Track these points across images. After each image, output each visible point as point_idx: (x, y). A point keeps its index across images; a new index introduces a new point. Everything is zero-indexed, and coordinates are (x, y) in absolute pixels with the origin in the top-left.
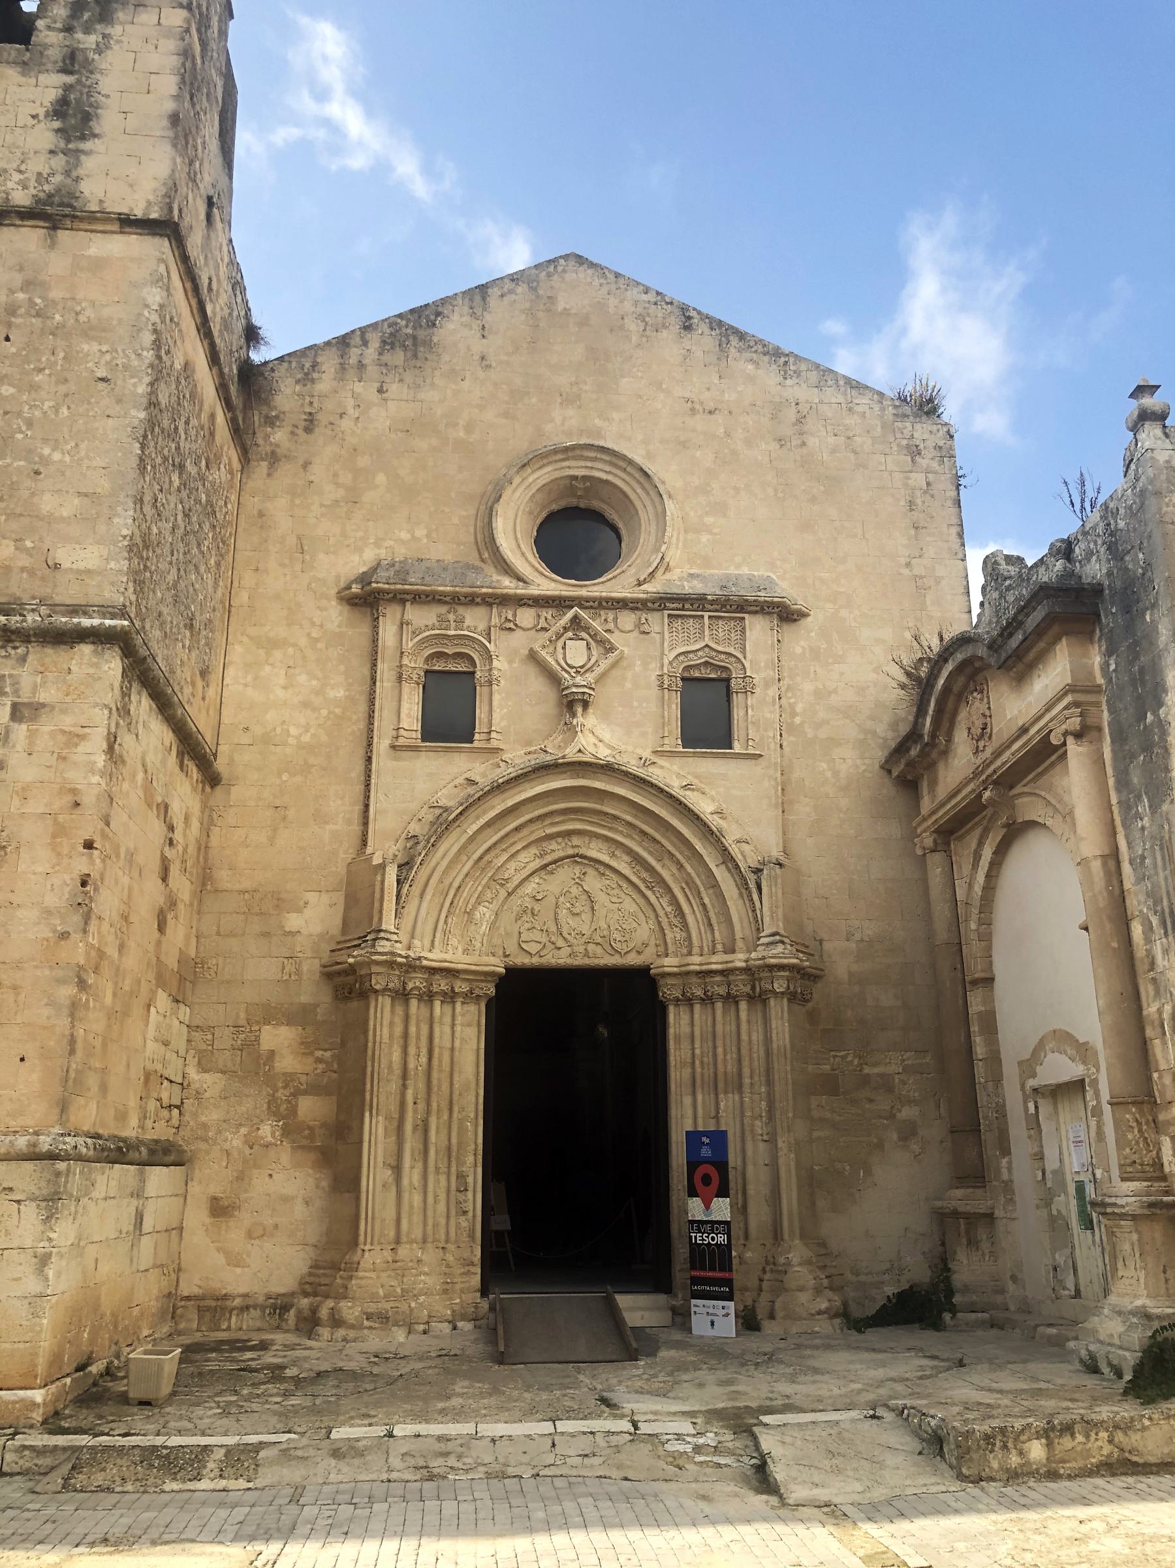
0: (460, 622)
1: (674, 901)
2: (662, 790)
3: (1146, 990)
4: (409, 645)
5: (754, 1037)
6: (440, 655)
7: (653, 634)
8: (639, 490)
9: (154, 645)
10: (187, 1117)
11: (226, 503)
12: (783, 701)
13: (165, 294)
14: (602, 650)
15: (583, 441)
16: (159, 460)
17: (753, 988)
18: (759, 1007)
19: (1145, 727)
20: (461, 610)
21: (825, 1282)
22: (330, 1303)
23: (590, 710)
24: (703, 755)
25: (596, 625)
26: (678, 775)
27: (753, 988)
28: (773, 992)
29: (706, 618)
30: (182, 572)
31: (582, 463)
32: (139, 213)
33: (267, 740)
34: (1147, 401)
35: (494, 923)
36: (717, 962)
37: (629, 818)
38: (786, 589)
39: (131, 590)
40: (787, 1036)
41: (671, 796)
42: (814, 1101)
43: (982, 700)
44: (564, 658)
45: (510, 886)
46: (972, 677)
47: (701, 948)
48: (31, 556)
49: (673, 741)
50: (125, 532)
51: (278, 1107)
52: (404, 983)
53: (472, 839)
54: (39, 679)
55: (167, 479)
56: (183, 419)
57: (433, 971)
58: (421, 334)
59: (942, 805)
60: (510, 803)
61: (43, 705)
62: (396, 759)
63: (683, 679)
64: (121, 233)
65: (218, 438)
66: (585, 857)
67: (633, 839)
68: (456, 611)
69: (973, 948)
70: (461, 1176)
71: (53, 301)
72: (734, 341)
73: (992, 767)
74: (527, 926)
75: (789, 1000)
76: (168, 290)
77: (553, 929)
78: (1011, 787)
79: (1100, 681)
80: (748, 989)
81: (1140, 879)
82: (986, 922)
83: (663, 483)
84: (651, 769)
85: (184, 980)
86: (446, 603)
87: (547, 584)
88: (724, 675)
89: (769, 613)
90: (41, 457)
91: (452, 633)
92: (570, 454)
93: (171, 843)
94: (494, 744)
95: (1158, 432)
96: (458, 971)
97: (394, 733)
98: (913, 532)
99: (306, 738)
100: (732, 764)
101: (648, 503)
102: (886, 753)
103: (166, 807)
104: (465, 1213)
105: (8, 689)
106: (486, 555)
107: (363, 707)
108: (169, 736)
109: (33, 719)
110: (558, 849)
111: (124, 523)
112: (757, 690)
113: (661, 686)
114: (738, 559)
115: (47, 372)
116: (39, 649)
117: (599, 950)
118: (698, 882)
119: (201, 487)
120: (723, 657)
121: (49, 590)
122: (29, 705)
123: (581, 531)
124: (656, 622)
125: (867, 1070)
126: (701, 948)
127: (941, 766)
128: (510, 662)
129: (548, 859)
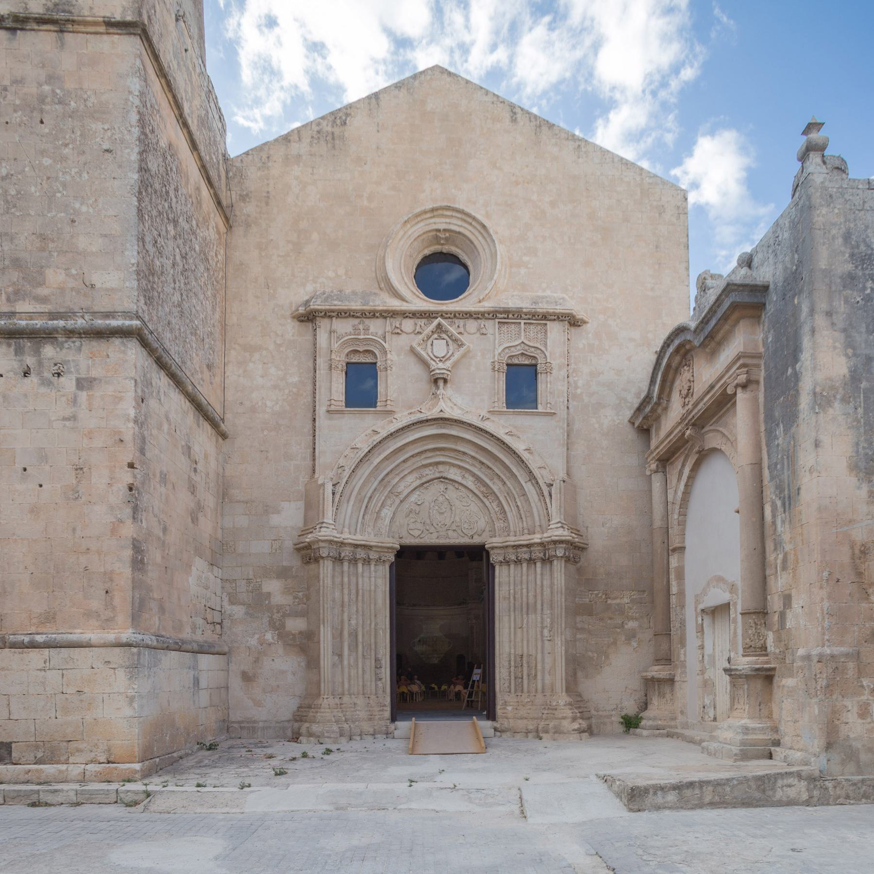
0: (367, 329)
1: (500, 504)
2: (493, 436)
3: (770, 546)
4: (335, 346)
5: (545, 583)
6: (356, 352)
7: (488, 335)
8: (480, 238)
9: (167, 344)
10: (225, 629)
11: (216, 255)
12: (571, 379)
13: (143, 84)
14: (456, 346)
15: (445, 204)
16: (154, 213)
17: (545, 555)
18: (548, 566)
19: (787, 377)
20: (367, 321)
21: (578, 715)
22: (307, 725)
23: (449, 385)
24: (519, 413)
25: (452, 330)
26: (503, 427)
27: (545, 555)
28: (556, 556)
29: (522, 324)
30: (184, 297)
31: (444, 220)
32: (118, 18)
33: (253, 410)
34: (814, 136)
35: (392, 518)
36: (524, 539)
37: (473, 454)
38: (572, 305)
39: (143, 302)
40: (563, 581)
41: (498, 439)
42: (578, 619)
43: (689, 371)
44: (432, 352)
45: (402, 497)
46: (684, 356)
47: (515, 532)
48: (76, 280)
49: (501, 405)
50: (133, 261)
51: (275, 623)
52: (340, 553)
53: (377, 467)
54: (90, 362)
55: (164, 229)
56: (173, 187)
57: (356, 546)
58: (337, 131)
59: (662, 442)
60: (399, 444)
61: (95, 379)
62: (330, 419)
63: (507, 365)
64: (108, 33)
65: (204, 206)
66: (446, 479)
67: (475, 466)
68: (364, 323)
69: (674, 531)
70: (377, 660)
71: (68, 91)
72: (545, 129)
73: (693, 413)
74: (412, 520)
75: (566, 561)
76: (145, 81)
77: (428, 522)
78: (703, 428)
79: (762, 350)
80: (542, 555)
81: (772, 478)
82: (683, 514)
83: (497, 233)
84: (487, 422)
85: (219, 552)
86: (358, 317)
87: (422, 303)
88: (534, 362)
89: (562, 321)
90: (74, 209)
91: (362, 337)
92: (435, 213)
93: (195, 470)
94: (389, 408)
95: (818, 160)
96: (371, 546)
97: (328, 403)
98: (657, 267)
99: (277, 408)
100: (537, 419)
101: (486, 247)
102: (632, 412)
103: (189, 448)
104: (380, 679)
105: (72, 370)
106: (382, 285)
107: (310, 387)
108: (187, 405)
109: (90, 388)
110: (430, 473)
111: (132, 255)
112: (554, 372)
113: (493, 369)
114: (544, 285)
115: (71, 146)
116: (88, 342)
117: (455, 534)
118: (514, 492)
119: (194, 240)
120: (533, 349)
121: (89, 303)
122: (85, 379)
123: (443, 270)
124: (491, 326)
125: (609, 601)
126: (515, 532)
127: (663, 418)
128: (398, 355)
129: (424, 480)
